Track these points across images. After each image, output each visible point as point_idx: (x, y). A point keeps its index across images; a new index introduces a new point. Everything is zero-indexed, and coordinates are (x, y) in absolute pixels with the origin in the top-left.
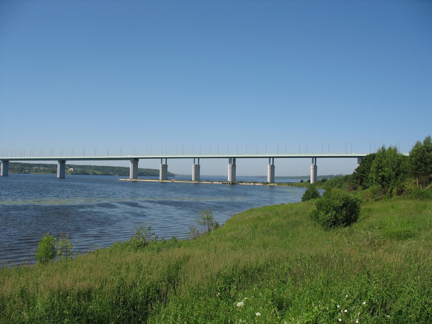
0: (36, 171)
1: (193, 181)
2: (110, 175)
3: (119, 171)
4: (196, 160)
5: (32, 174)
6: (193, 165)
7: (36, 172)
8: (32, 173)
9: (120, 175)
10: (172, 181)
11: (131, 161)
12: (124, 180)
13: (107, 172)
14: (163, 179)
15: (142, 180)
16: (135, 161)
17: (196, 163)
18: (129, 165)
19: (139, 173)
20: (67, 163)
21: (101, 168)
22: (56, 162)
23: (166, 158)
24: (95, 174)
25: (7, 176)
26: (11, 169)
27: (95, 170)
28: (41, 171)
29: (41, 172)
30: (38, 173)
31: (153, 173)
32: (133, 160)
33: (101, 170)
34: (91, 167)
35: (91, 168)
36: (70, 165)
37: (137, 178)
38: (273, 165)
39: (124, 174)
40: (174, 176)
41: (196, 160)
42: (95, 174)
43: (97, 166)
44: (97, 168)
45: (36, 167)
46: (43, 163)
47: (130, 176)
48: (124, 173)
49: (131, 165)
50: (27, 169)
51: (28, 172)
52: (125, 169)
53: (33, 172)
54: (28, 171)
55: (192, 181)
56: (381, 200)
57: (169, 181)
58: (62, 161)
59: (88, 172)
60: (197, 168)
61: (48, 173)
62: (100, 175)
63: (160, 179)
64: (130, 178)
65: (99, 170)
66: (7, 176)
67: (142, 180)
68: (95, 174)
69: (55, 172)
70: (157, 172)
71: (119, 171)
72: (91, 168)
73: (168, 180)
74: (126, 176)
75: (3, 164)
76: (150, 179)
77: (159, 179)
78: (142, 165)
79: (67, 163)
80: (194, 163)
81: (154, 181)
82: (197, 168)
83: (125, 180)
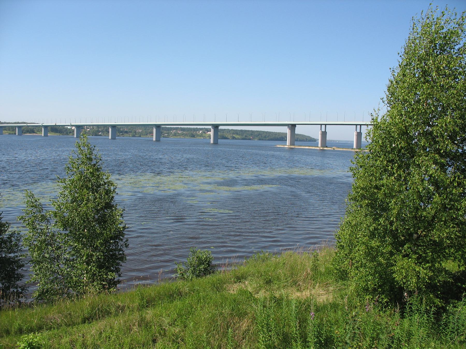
0: (175, 135)
1: (354, 149)
2: (250, 139)
3: (258, 135)
4: (323, 126)
5: (172, 138)
6: (320, 132)
7: (175, 136)
8: (171, 137)
9: (260, 140)
10: (334, 149)
11: (289, 128)
12: (282, 146)
13: (246, 136)
14: (322, 146)
15: (301, 147)
16: (293, 127)
17: (323, 130)
18: (287, 130)
19: (296, 138)
20: (221, 127)
21: (239, 132)
22: (210, 127)
23: (326, 125)
24: (234, 139)
25: (47, 136)
26: (151, 133)
27: (233, 134)
28: (179, 135)
29: (179, 136)
30: (177, 137)
31: (310, 140)
32: (290, 126)
33: (240, 134)
34: (229, 131)
35: (229, 132)
36: (207, 128)
37: (294, 145)
38: (360, 132)
39: (264, 139)
40: (316, 141)
41: (323, 126)
42: (234, 138)
43: (269, 132)
44: (236, 132)
45: (174, 131)
46: (206, 128)
47: (287, 141)
48: (264, 138)
49: (289, 131)
50: (166, 133)
51: (167, 136)
52: (265, 133)
53: (171, 136)
54: (167, 135)
55: (318, 147)
56: (104, 158)
57: (330, 149)
58: (216, 127)
59: (226, 136)
60: (324, 134)
61: (187, 137)
62: (239, 139)
63: (319, 146)
64: (287, 145)
65: (237, 134)
66: (115, 139)
67: (301, 147)
68: (234, 139)
69: (74, 135)
70: (298, 137)
71: (258, 135)
72: (229, 132)
73: (327, 147)
74: (266, 140)
75: (155, 129)
76: (310, 146)
77: (318, 147)
78: (299, 130)
79: (221, 127)
80: (321, 129)
81: (313, 148)
82: (324, 134)
83: (283, 146)
